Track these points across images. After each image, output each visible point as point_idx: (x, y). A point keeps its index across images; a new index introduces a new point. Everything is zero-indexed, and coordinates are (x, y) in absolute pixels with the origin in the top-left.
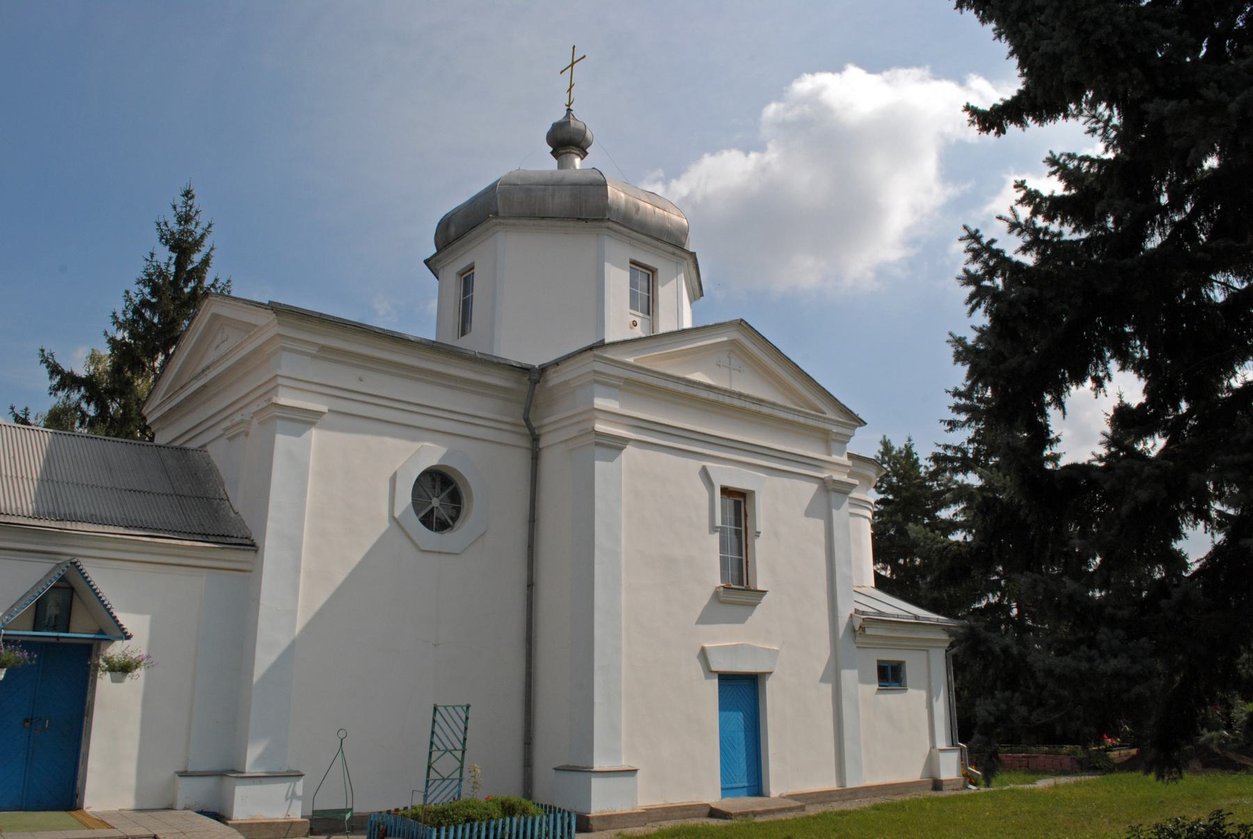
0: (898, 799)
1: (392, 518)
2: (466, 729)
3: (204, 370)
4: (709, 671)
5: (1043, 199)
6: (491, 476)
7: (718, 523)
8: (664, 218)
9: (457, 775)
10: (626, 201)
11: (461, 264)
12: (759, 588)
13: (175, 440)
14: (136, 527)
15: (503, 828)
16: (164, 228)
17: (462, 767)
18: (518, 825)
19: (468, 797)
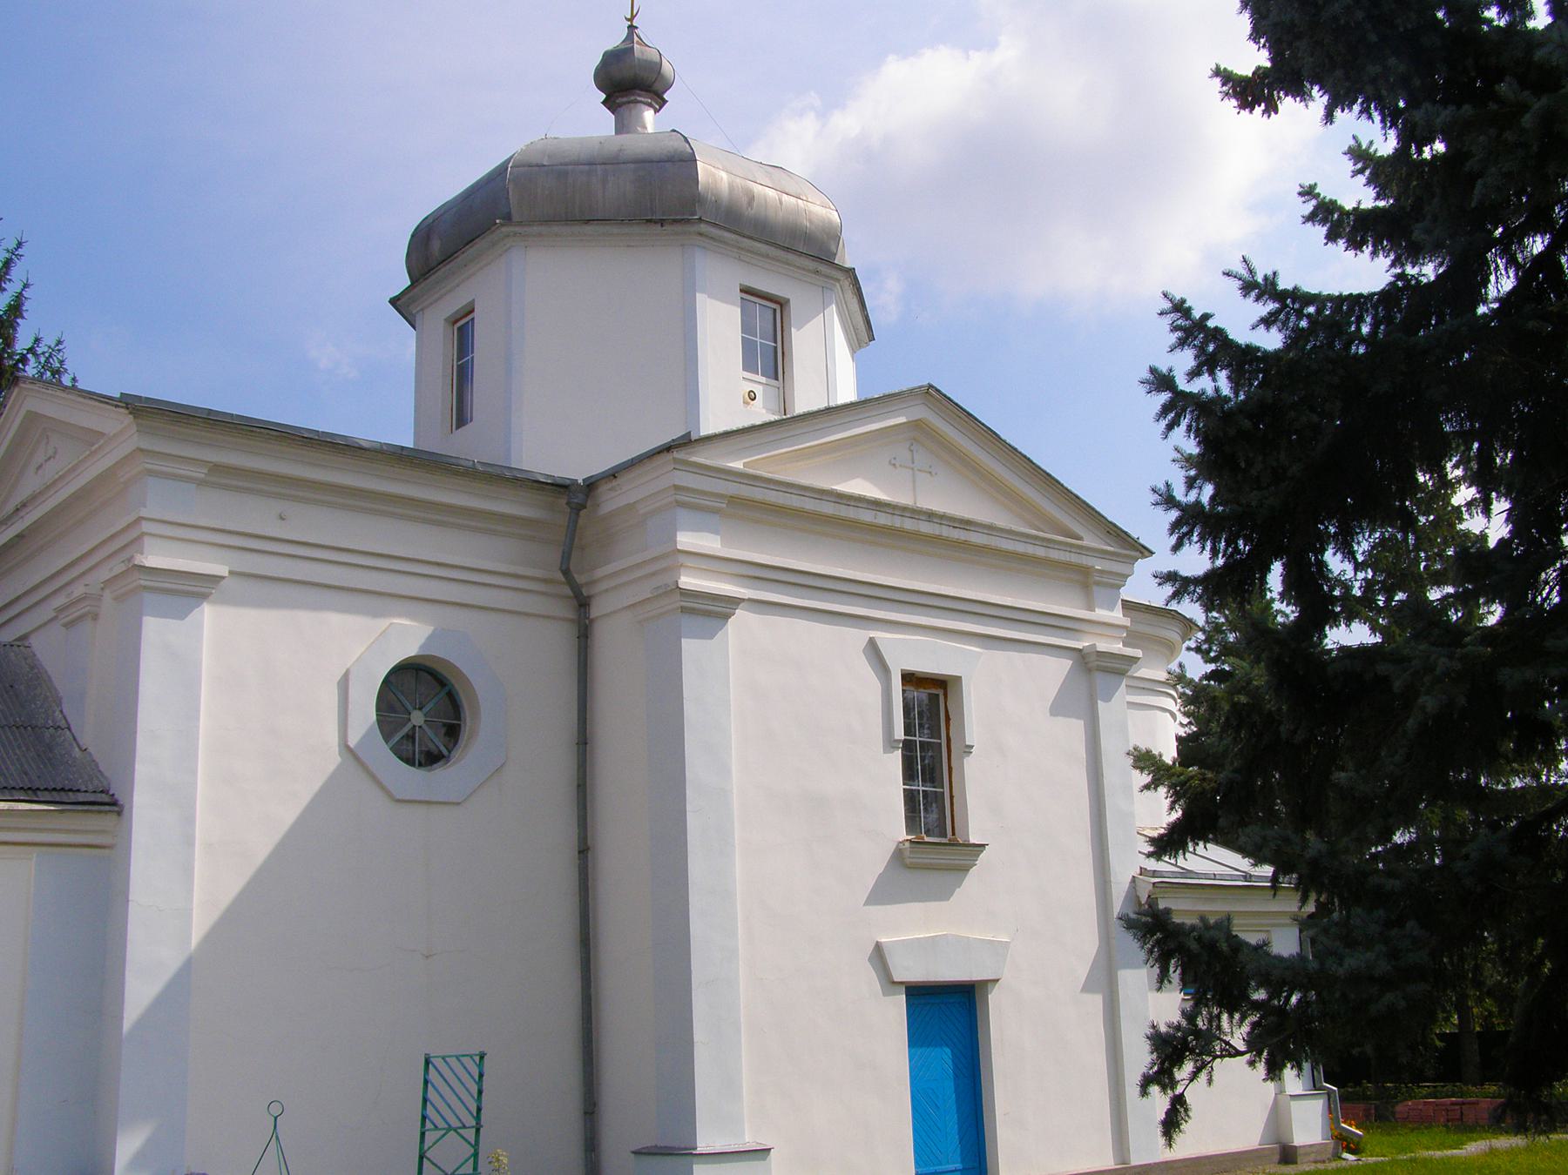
2: (480, 1092)
4: (890, 983)
6: (510, 670)
7: (899, 733)
10: (731, 187)
11: (452, 304)
12: (973, 840)
17: (476, 1155)
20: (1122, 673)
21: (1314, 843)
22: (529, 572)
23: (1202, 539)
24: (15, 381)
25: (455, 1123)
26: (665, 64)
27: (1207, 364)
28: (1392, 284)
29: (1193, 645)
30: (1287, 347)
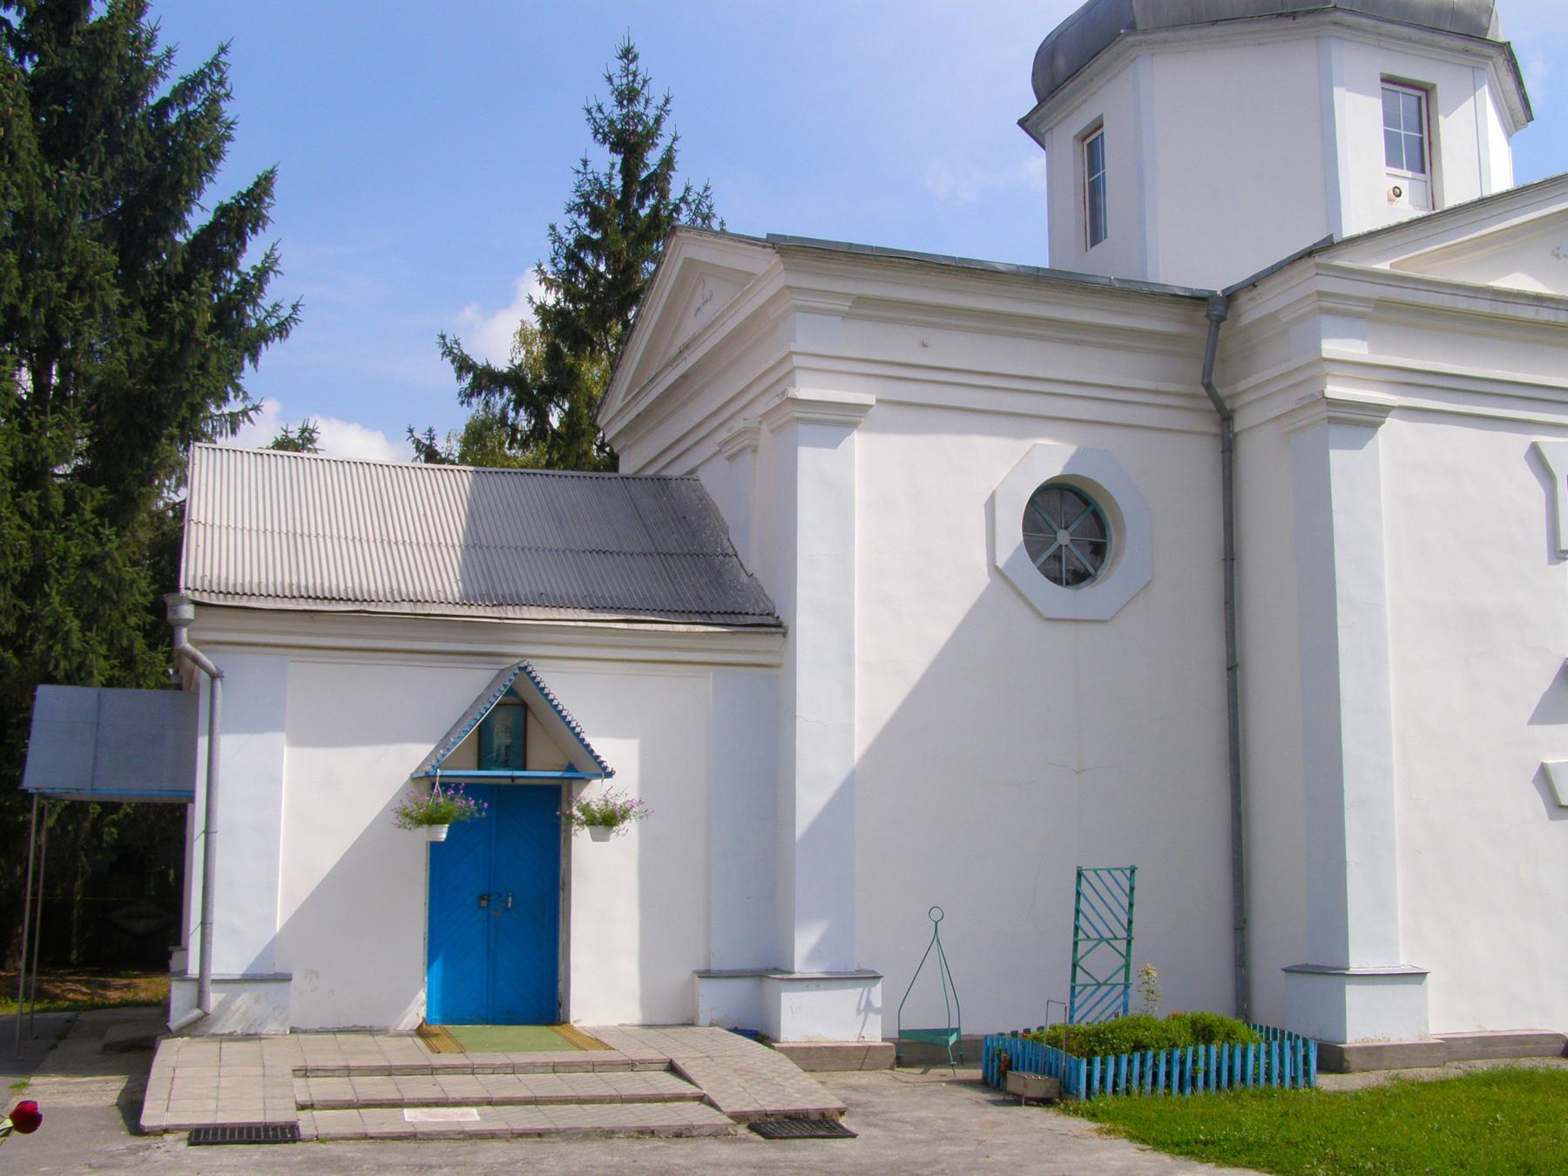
1: (994, 568)
2: (1131, 905)
6: (1156, 487)
9: (1120, 978)
11: (1081, 120)
13: (650, 463)
14: (604, 609)
15: (1195, 1062)
17: (1127, 966)
18: (1219, 1056)
19: (1138, 1013)
24: (674, 229)
25: (1107, 935)
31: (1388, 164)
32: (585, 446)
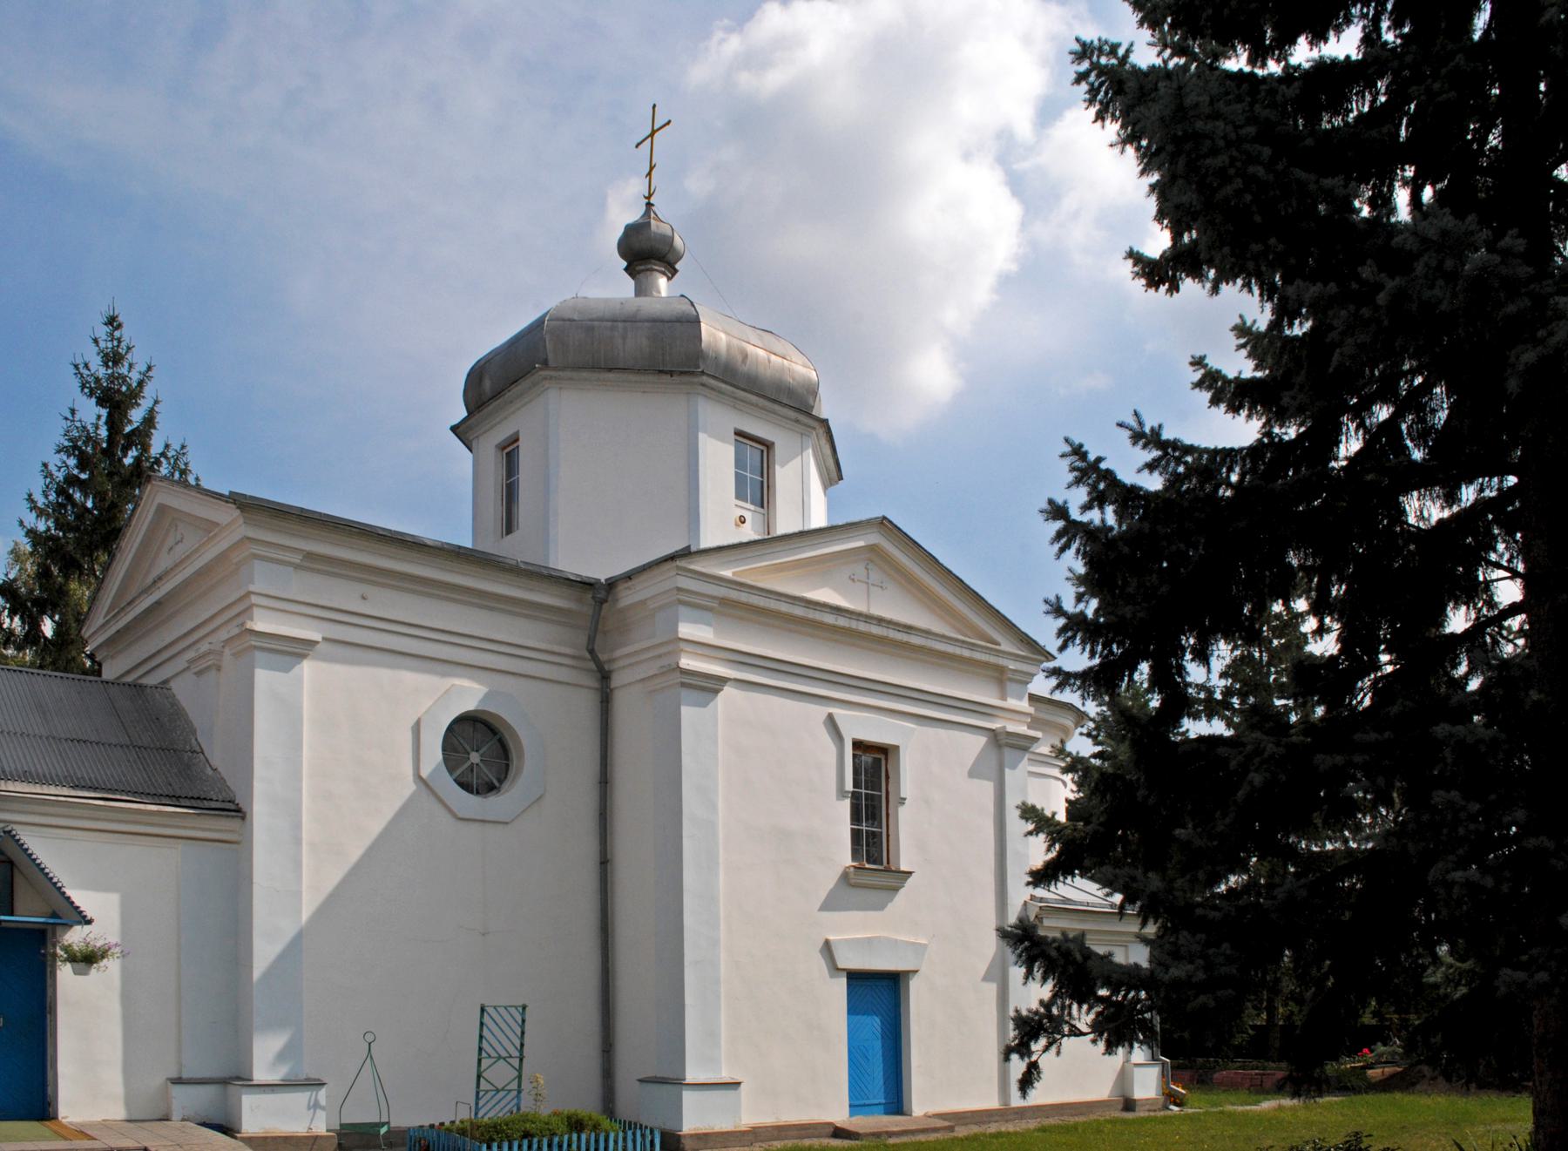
0: (1073, 1120)
1: (418, 777)
3: (129, 604)
4: (835, 969)
5: (1226, 381)
6: (548, 722)
7: (849, 786)
8: (783, 368)
9: (514, 1085)
10: (729, 346)
11: (501, 434)
12: (903, 868)
13: (128, 672)
14: (83, 788)
16: (86, 372)
17: (520, 1077)
20: (1026, 749)
21: (1155, 882)
22: (568, 651)
23: (1083, 642)
24: (149, 478)
25: (504, 1054)
26: (677, 238)
27: (1097, 500)
28: (1259, 441)
29: (1085, 731)
30: (1166, 489)
31: (738, 497)
32: (74, 653)
